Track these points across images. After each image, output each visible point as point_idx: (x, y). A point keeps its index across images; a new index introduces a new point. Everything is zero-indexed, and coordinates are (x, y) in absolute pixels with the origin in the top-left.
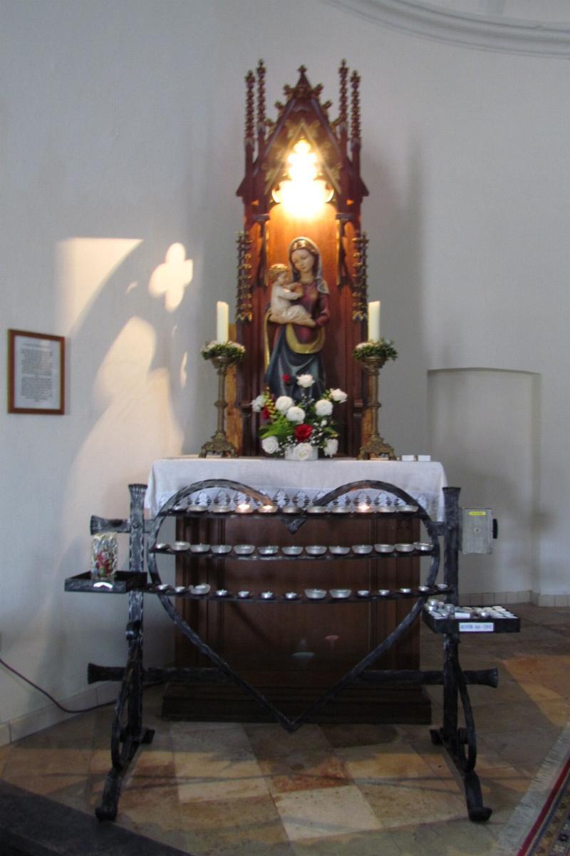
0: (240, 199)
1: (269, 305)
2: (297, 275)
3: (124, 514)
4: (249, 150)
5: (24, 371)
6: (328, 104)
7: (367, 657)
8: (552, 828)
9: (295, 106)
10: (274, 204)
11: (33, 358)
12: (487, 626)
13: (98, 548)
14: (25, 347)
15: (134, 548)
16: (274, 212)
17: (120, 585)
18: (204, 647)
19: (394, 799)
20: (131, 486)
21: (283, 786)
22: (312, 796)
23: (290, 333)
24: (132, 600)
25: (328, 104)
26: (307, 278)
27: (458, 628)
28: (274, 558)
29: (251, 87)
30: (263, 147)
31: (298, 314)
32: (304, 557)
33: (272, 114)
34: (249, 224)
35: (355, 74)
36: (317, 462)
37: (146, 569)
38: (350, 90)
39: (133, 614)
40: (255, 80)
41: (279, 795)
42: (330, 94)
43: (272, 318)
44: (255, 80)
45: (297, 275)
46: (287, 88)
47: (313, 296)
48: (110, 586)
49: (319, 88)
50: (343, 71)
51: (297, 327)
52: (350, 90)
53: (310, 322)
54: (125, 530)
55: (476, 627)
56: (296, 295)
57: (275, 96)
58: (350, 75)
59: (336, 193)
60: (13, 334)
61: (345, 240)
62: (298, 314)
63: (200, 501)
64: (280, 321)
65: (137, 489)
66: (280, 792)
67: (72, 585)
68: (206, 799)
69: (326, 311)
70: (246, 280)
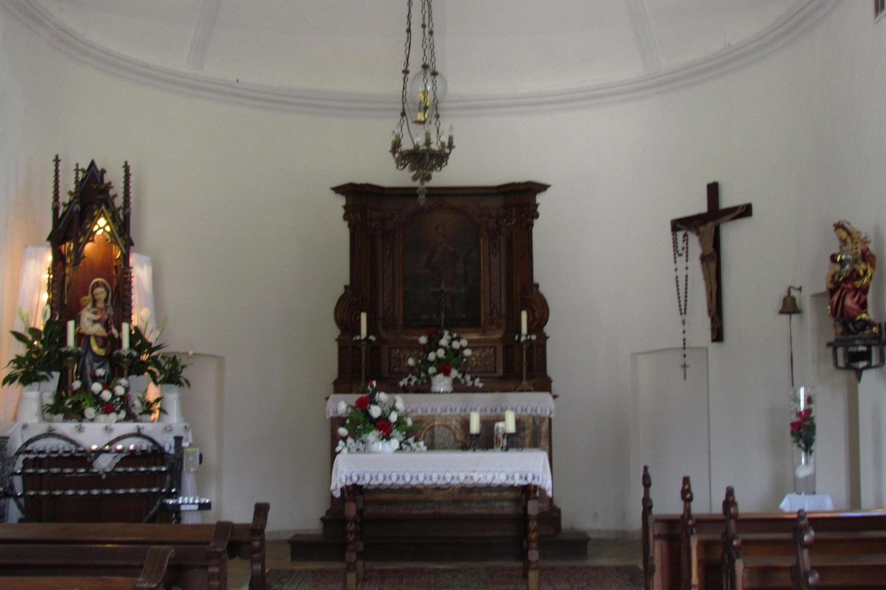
47: (106, 317)
51: (96, 337)
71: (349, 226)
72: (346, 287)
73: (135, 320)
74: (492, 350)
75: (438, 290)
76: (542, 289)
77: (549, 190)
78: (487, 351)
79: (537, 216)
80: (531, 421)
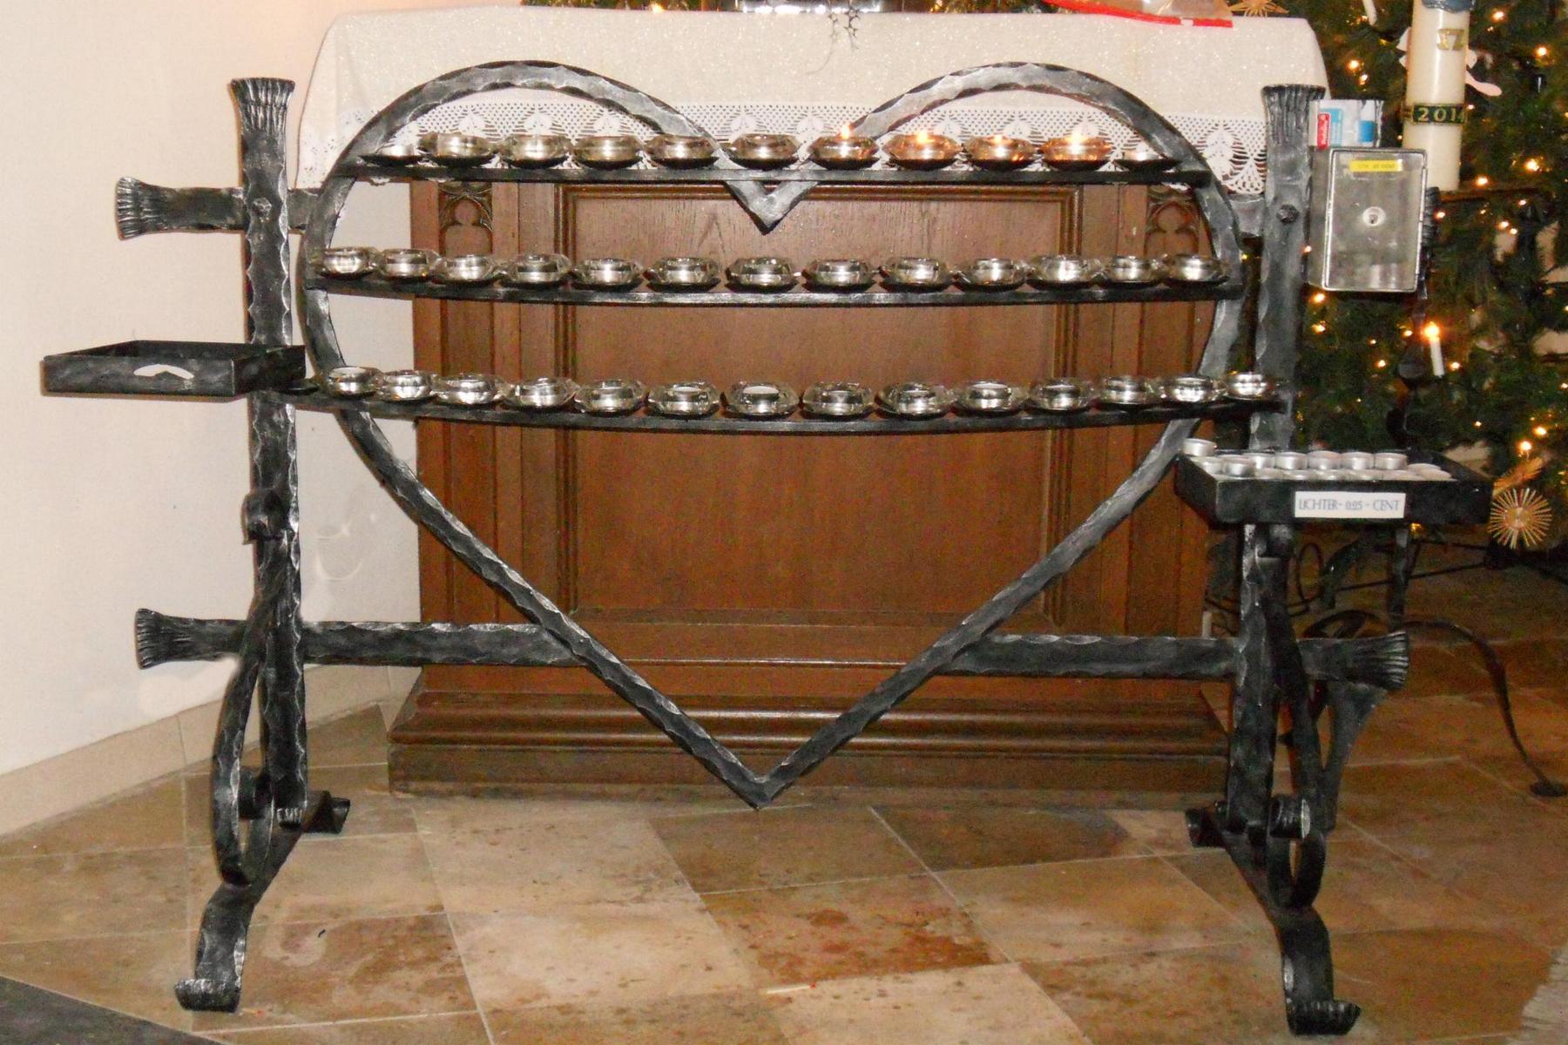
7: (1440, 760)
12: (1384, 503)
13: (1230, 708)
15: (259, 273)
17: (217, 371)
18: (490, 562)
19: (1136, 1001)
20: (238, 88)
21: (790, 965)
22: (882, 994)
24: (262, 430)
27: (1290, 507)
28: (706, 298)
32: (726, 297)
36: (522, 9)
39: (264, 467)
41: (783, 991)
48: (186, 375)
54: (230, 221)
55: (1349, 506)
63: (460, 126)
65: (258, 104)
66: (785, 982)
67: (67, 372)
68: (557, 1001)
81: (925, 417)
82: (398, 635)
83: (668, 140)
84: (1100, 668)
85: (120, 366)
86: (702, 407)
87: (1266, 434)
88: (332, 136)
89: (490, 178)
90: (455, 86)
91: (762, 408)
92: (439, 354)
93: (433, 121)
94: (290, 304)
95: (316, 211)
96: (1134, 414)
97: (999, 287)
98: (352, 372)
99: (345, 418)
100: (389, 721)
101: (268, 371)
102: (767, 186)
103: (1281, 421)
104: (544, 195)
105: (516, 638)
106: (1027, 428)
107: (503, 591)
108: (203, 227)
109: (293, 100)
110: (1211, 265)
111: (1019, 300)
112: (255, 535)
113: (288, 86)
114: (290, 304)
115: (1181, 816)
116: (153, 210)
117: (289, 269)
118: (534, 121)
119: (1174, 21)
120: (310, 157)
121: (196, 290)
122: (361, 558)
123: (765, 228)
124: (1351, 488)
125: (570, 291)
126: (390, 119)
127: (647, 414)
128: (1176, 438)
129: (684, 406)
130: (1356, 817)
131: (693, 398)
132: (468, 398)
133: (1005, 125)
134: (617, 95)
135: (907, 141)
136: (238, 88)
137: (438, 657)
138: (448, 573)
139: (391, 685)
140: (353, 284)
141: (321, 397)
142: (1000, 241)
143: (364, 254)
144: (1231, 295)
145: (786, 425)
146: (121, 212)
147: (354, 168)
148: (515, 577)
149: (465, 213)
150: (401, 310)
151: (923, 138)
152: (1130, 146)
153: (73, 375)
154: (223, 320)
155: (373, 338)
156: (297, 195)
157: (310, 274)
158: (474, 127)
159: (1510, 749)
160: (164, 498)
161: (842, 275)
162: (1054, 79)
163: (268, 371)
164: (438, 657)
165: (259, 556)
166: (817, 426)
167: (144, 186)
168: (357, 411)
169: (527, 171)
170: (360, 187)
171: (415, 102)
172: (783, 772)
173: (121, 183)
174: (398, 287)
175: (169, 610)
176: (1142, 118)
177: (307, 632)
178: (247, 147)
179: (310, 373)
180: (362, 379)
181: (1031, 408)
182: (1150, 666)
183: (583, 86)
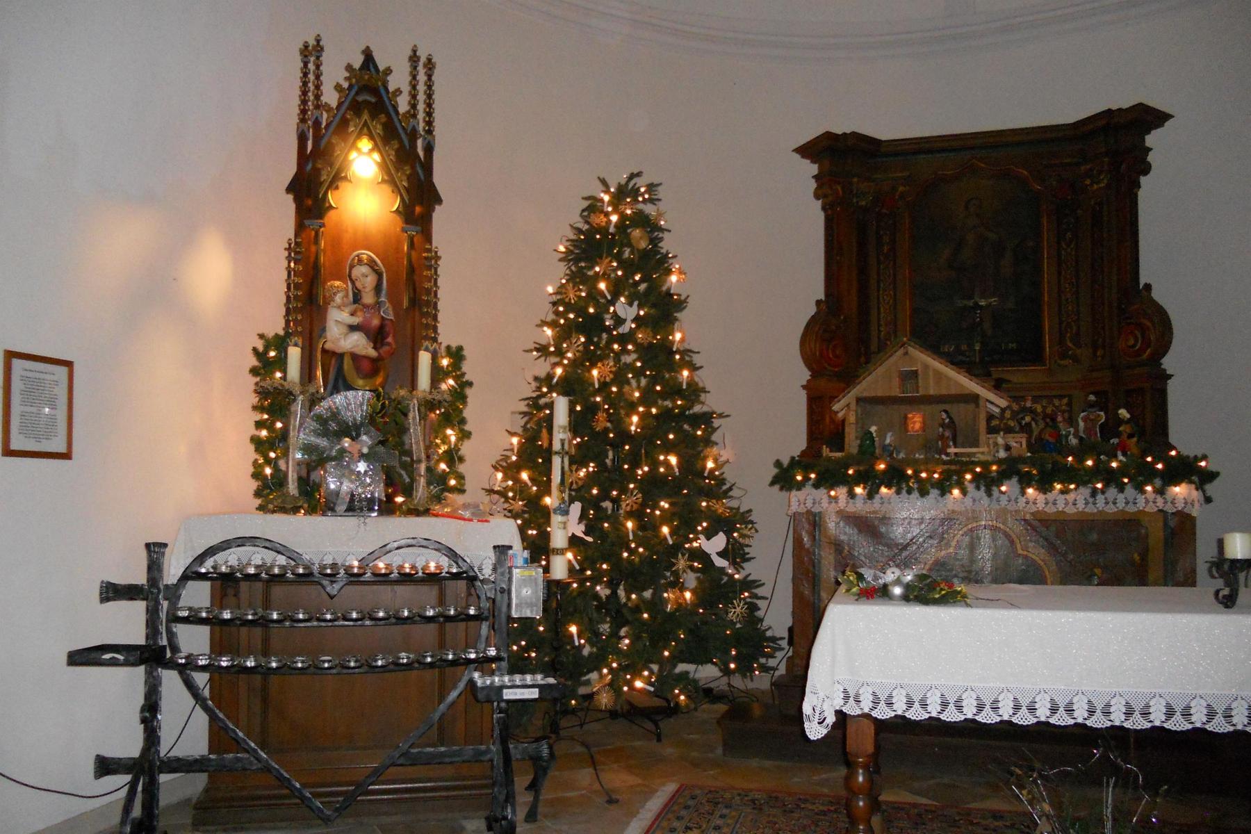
0: (290, 197)
1: (324, 330)
2: (357, 298)
3: (140, 578)
4: (302, 139)
5: (24, 403)
6: (398, 92)
8: (665, 824)
9: (357, 93)
10: (331, 207)
11: (35, 392)
14: (25, 373)
16: (331, 217)
20: (148, 546)
23: (347, 364)
25: (398, 92)
26: (368, 298)
28: (309, 624)
29: (306, 64)
30: (317, 138)
31: (357, 343)
32: (342, 623)
33: (330, 97)
34: (300, 227)
35: (429, 60)
37: (164, 642)
38: (422, 77)
40: (312, 53)
42: (398, 80)
43: (327, 346)
44: (312, 53)
45: (357, 298)
46: (349, 68)
47: (376, 322)
48: (121, 657)
49: (388, 71)
50: (414, 58)
51: (355, 357)
52: (422, 77)
53: (373, 353)
56: (355, 320)
57: (334, 75)
58: (423, 60)
59: (402, 200)
60: (11, 355)
61: (413, 253)
62: (357, 343)
63: (229, 560)
64: (339, 351)
65: (155, 551)
69: (390, 339)
70: (296, 297)
71: (824, 208)
72: (818, 302)
73: (448, 334)
74: (1065, 401)
75: (971, 303)
76: (1156, 295)
77: (770, 479)
78: (1057, 402)
79: (1146, 169)
80: (1160, 524)
81: (382, 666)
82: (196, 761)
83: (297, 566)
84: (447, 760)
85: (93, 655)
86: (306, 665)
87: (499, 669)
88: (182, 562)
89: (237, 580)
90: (225, 546)
91: (326, 665)
92: (218, 648)
93: (220, 557)
94: (163, 629)
95: (173, 593)
96: (454, 663)
97: (407, 618)
98: (182, 655)
99: (181, 673)
100: (194, 801)
101: (151, 656)
102: (332, 582)
103: (504, 664)
104: (259, 586)
105: (238, 760)
106: (418, 669)
107: (237, 740)
108: (132, 599)
109: (167, 550)
110: (478, 608)
111: (415, 623)
112: (144, 721)
113: (165, 545)
114: (163, 629)
115: (483, 820)
116: (112, 592)
117: (163, 616)
118: (256, 558)
119: (471, 520)
120: (173, 570)
121: (127, 624)
122: (186, 729)
123: (332, 597)
124: (522, 689)
125: (264, 622)
126: (201, 559)
127: (314, 669)
128: (470, 672)
129: (300, 665)
130: (545, 816)
131: (303, 662)
132: (224, 664)
133: (406, 561)
134: (281, 549)
135: (376, 566)
136: (148, 546)
137: (211, 769)
138: (219, 737)
139: (199, 781)
140: (185, 620)
141: (171, 665)
142: (405, 601)
143: (190, 609)
144: (486, 619)
145: (334, 671)
146: (101, 594)
147: (190, 575)
148: (241, 734)
149: (230, 591)
150: (205, 630)
151: (381, 565)
152: (450, 566)
153: (80, 658)
154: (136, 635)
155: (194, 641)
156: (167, 586)
157: (171, 617)
158: (233, 561)
159: (599, 788)
160: (108, 710)
161: (354, 615)
162: (426, 544)
163: (151, 656)
164: (211, 769)
165: (146, 730)
166: (345, 671)
167: (109, 583)
168: (186, 669)
169: (248, 577)
170: (190, 583)
171: (211, 551)
172: (337, 810)
173: (261, 508)
174: (202, 621)
175: (106, 755)
176: (453, 555)
177: (162, 762)
178: (150, 568)
179: (169, 655)
180: (186, 658)
181: (441, 660)
182: (465, 758)
183: (270, 545)
